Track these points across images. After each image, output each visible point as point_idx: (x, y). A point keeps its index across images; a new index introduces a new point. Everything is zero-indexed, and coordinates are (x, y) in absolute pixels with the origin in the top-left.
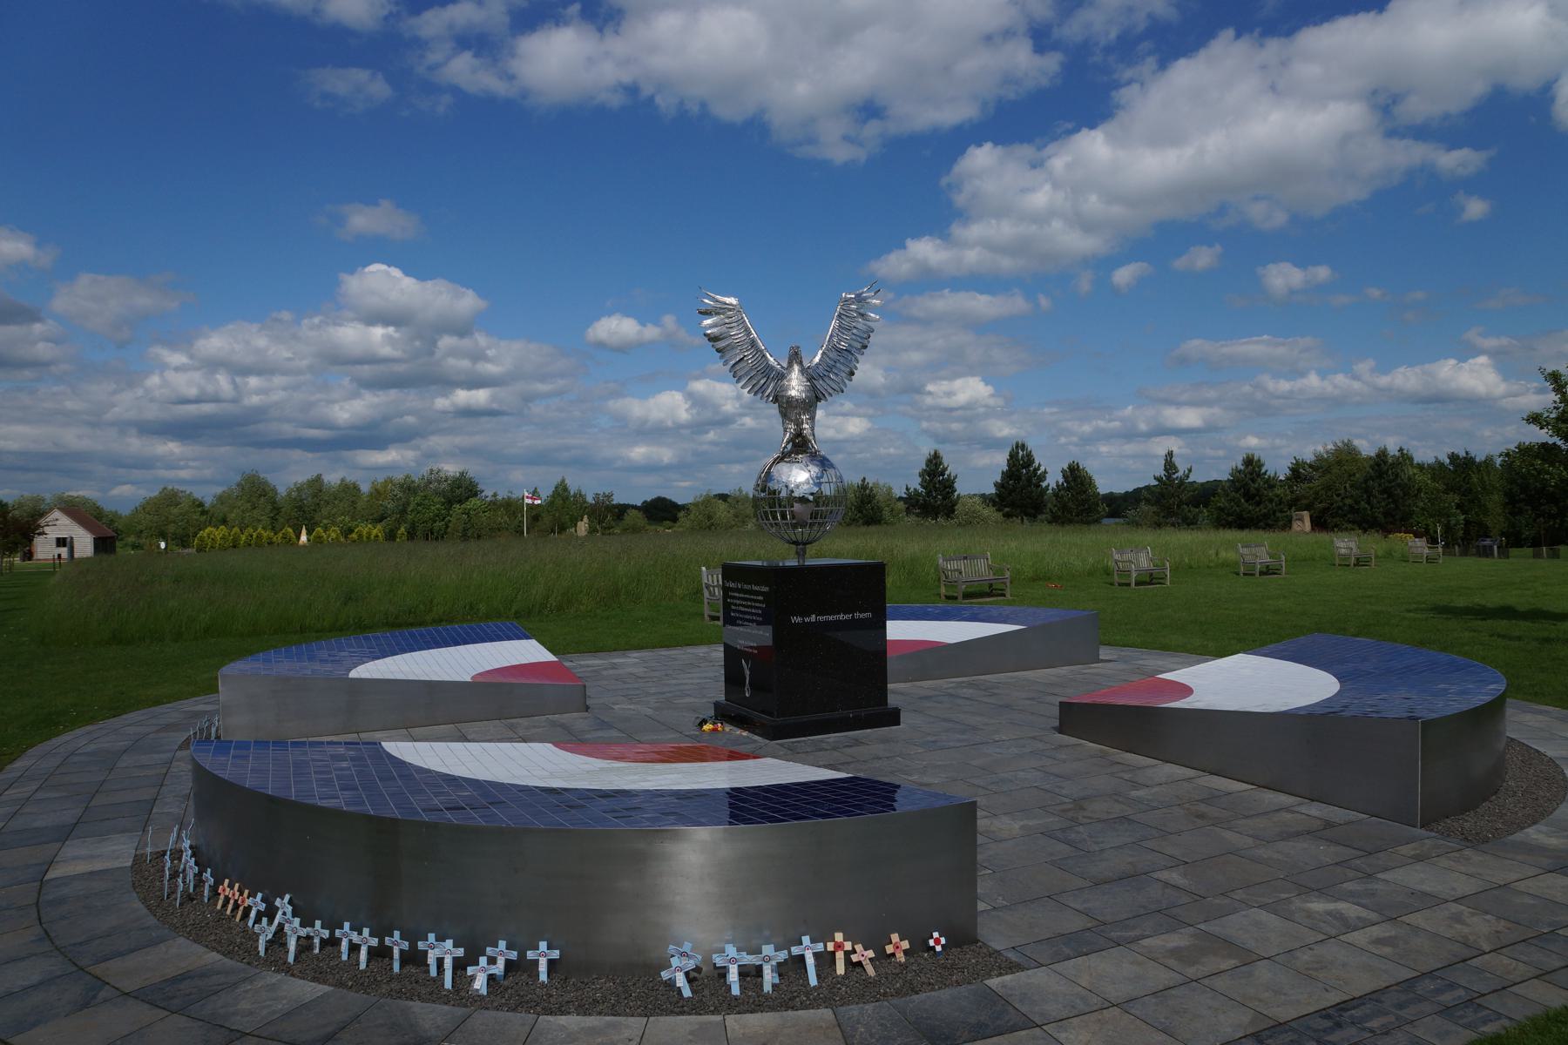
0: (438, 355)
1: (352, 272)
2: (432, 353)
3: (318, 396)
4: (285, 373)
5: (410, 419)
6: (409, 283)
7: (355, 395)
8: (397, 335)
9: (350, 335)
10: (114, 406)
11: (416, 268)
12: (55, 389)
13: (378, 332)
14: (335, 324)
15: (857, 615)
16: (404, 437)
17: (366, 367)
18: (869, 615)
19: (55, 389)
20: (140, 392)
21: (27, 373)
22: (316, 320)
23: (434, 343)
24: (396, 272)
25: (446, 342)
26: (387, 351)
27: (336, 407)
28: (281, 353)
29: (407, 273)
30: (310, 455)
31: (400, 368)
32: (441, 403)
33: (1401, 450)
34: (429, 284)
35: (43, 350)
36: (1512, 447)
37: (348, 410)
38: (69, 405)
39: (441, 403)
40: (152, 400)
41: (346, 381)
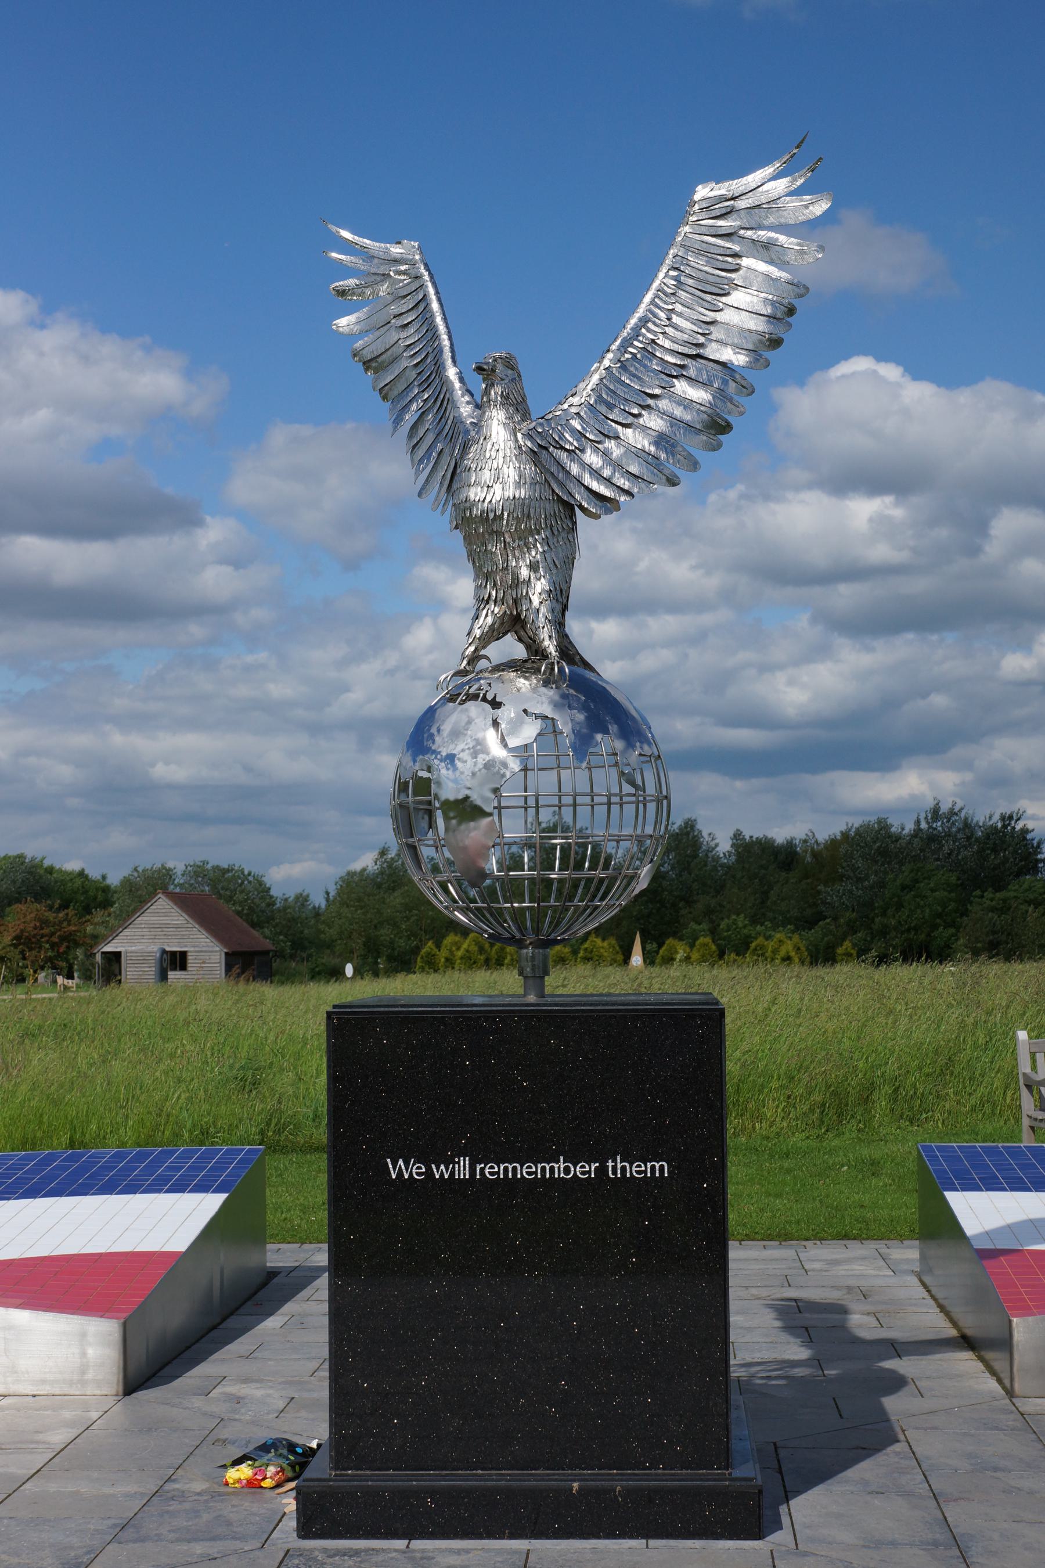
0: (993, 551)
1: (801, 383)
2: (974, 551)
3: (744, 656)
4: (676, 606)
5: (939, 701)
6: (919, 394)
7: (821, 652)
8: (898, 513)
9: (804, 519)
10: (347, 689)
11: (935, 361)
12: (250, 659)
13: (863, 510)
14: (767, 498)
15: (616, 1166)
16: (930, 743)
17: (843, 588)
18: (660, 1167)
19: (250, 659)
20: (393, 659)
21: (196, 630)
22: (732, 494)
23: (982, 528)
24: (891, 372)
25: (1010, 524)
26: (881, 553)
27: (780, 678)
28: (679, 572)
29: (916, 372)
30: (739, 784)
31: (918, 586)
32: (1016, 664)
33: (1039, 844)
34: (964, 397)
35: (215, 581)
36: (344, 874)
37: (809, 685)
38: (279, 690)
39: (1016, 664)
40: (416, 676)
41: (802, 621)
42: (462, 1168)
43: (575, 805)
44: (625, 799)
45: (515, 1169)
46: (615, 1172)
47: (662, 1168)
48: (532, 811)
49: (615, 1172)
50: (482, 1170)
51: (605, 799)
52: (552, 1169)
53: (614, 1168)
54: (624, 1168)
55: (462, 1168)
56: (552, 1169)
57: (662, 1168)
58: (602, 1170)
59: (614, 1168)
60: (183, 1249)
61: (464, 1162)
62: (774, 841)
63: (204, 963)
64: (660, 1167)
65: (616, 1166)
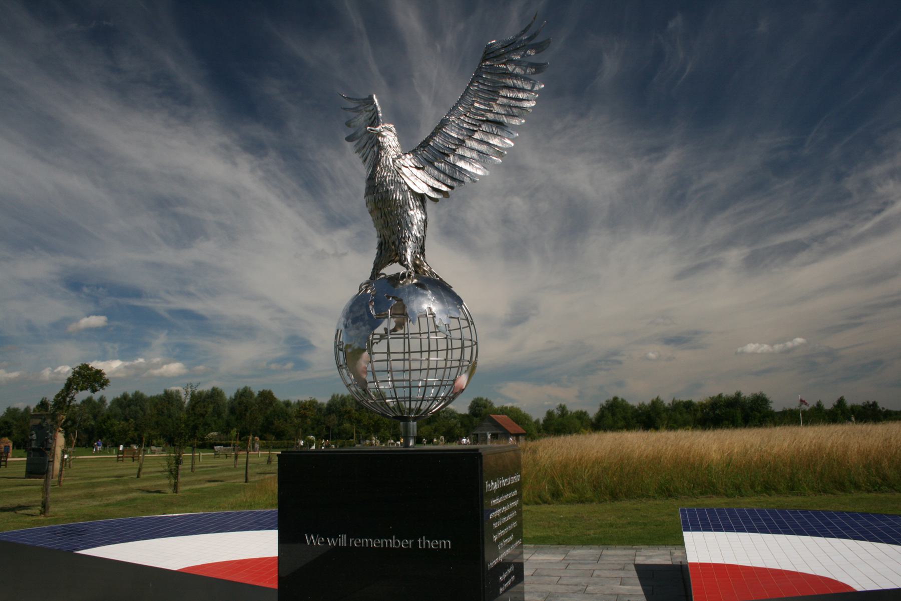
15: (423, 542)
18: (447, 543)
42: (343, 540)
43: (404, 360)
44: (393, 356)
45: (369, 542)
46: (422, 545)
47: (447, 543)
48: (449, 357)
49: (422, 545)
50: (353, 542)
51: (393, 356)
52: (389, 542)
53: (422, 543)
54: (427, 543)
55: (343, 540)
56: (389, 542)
57: (447, 543)
58: (415, 544)
59: (422, 543)
60: (858, 588)
61: (344, 537)
62: (492, 405)
63: (93, 485)
64: (447, 543)
65: (423, 542)
